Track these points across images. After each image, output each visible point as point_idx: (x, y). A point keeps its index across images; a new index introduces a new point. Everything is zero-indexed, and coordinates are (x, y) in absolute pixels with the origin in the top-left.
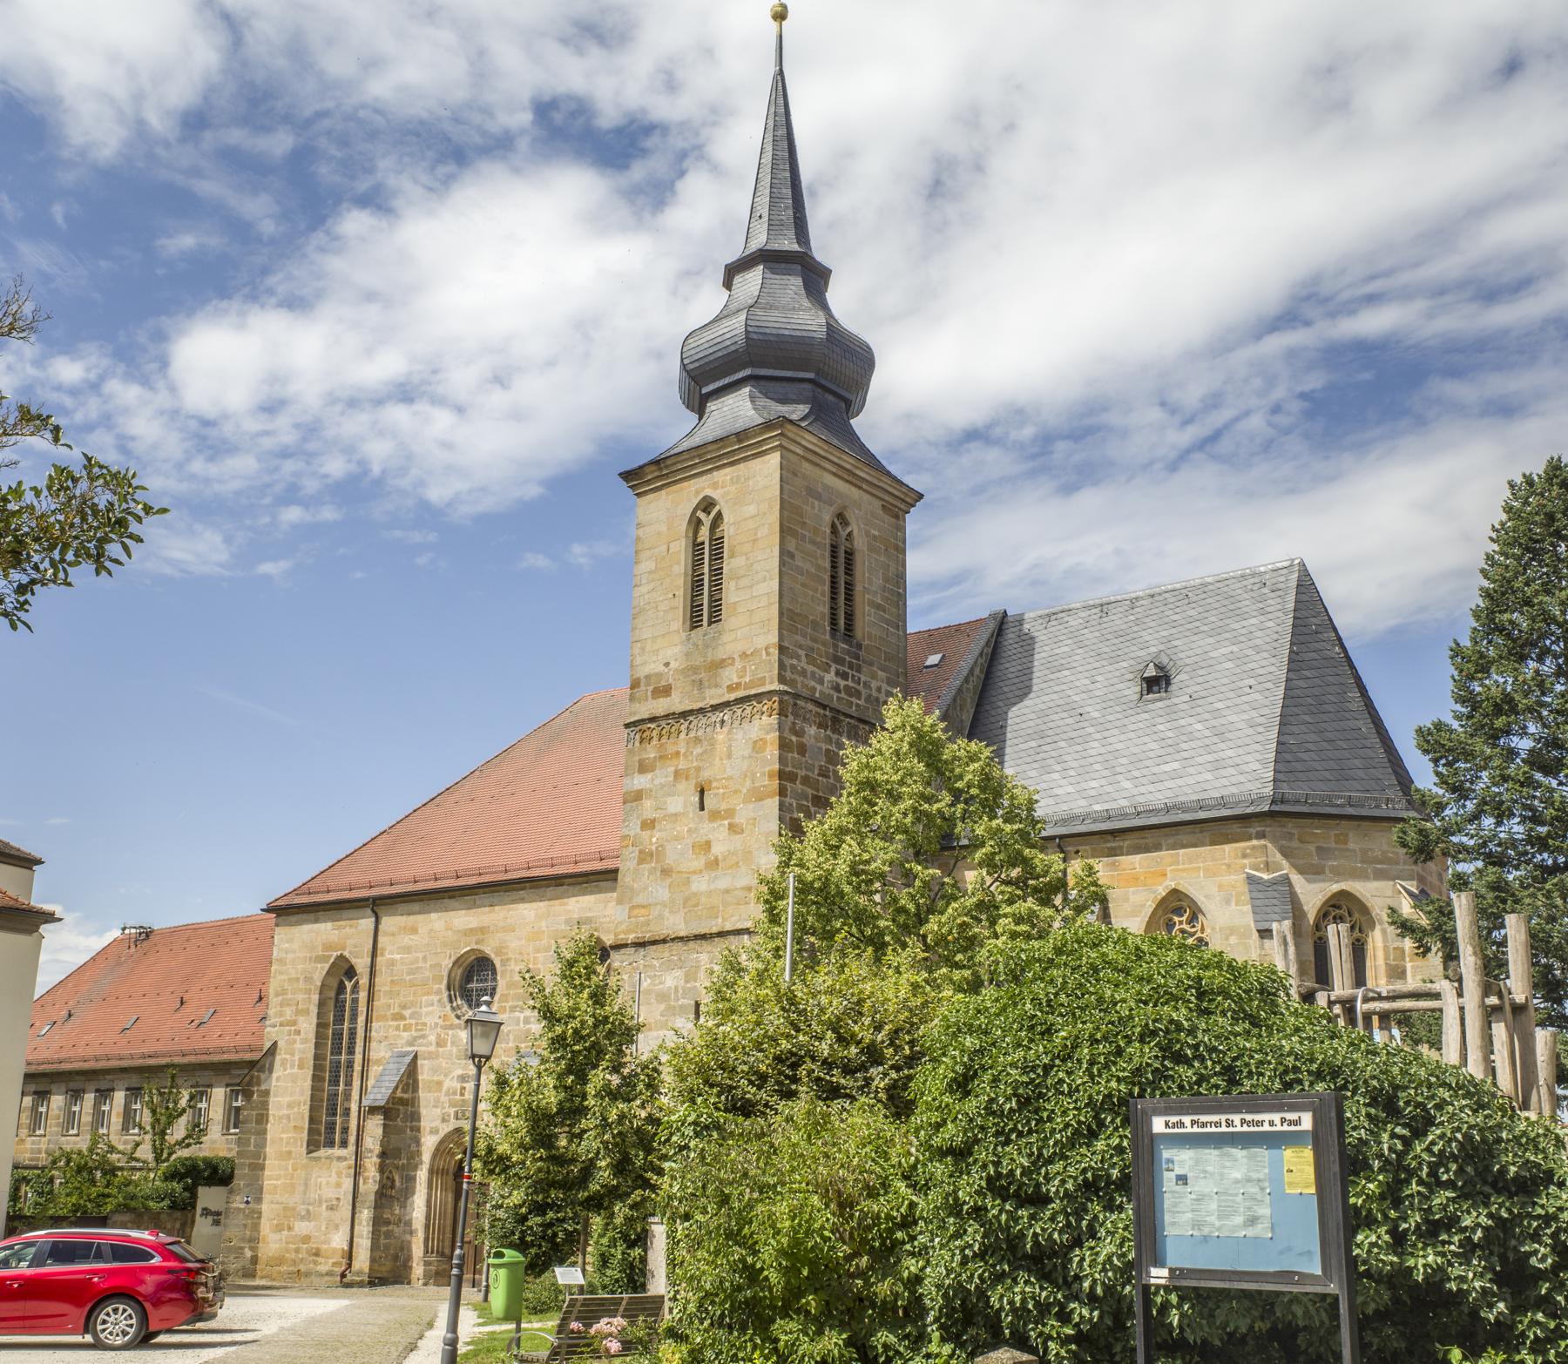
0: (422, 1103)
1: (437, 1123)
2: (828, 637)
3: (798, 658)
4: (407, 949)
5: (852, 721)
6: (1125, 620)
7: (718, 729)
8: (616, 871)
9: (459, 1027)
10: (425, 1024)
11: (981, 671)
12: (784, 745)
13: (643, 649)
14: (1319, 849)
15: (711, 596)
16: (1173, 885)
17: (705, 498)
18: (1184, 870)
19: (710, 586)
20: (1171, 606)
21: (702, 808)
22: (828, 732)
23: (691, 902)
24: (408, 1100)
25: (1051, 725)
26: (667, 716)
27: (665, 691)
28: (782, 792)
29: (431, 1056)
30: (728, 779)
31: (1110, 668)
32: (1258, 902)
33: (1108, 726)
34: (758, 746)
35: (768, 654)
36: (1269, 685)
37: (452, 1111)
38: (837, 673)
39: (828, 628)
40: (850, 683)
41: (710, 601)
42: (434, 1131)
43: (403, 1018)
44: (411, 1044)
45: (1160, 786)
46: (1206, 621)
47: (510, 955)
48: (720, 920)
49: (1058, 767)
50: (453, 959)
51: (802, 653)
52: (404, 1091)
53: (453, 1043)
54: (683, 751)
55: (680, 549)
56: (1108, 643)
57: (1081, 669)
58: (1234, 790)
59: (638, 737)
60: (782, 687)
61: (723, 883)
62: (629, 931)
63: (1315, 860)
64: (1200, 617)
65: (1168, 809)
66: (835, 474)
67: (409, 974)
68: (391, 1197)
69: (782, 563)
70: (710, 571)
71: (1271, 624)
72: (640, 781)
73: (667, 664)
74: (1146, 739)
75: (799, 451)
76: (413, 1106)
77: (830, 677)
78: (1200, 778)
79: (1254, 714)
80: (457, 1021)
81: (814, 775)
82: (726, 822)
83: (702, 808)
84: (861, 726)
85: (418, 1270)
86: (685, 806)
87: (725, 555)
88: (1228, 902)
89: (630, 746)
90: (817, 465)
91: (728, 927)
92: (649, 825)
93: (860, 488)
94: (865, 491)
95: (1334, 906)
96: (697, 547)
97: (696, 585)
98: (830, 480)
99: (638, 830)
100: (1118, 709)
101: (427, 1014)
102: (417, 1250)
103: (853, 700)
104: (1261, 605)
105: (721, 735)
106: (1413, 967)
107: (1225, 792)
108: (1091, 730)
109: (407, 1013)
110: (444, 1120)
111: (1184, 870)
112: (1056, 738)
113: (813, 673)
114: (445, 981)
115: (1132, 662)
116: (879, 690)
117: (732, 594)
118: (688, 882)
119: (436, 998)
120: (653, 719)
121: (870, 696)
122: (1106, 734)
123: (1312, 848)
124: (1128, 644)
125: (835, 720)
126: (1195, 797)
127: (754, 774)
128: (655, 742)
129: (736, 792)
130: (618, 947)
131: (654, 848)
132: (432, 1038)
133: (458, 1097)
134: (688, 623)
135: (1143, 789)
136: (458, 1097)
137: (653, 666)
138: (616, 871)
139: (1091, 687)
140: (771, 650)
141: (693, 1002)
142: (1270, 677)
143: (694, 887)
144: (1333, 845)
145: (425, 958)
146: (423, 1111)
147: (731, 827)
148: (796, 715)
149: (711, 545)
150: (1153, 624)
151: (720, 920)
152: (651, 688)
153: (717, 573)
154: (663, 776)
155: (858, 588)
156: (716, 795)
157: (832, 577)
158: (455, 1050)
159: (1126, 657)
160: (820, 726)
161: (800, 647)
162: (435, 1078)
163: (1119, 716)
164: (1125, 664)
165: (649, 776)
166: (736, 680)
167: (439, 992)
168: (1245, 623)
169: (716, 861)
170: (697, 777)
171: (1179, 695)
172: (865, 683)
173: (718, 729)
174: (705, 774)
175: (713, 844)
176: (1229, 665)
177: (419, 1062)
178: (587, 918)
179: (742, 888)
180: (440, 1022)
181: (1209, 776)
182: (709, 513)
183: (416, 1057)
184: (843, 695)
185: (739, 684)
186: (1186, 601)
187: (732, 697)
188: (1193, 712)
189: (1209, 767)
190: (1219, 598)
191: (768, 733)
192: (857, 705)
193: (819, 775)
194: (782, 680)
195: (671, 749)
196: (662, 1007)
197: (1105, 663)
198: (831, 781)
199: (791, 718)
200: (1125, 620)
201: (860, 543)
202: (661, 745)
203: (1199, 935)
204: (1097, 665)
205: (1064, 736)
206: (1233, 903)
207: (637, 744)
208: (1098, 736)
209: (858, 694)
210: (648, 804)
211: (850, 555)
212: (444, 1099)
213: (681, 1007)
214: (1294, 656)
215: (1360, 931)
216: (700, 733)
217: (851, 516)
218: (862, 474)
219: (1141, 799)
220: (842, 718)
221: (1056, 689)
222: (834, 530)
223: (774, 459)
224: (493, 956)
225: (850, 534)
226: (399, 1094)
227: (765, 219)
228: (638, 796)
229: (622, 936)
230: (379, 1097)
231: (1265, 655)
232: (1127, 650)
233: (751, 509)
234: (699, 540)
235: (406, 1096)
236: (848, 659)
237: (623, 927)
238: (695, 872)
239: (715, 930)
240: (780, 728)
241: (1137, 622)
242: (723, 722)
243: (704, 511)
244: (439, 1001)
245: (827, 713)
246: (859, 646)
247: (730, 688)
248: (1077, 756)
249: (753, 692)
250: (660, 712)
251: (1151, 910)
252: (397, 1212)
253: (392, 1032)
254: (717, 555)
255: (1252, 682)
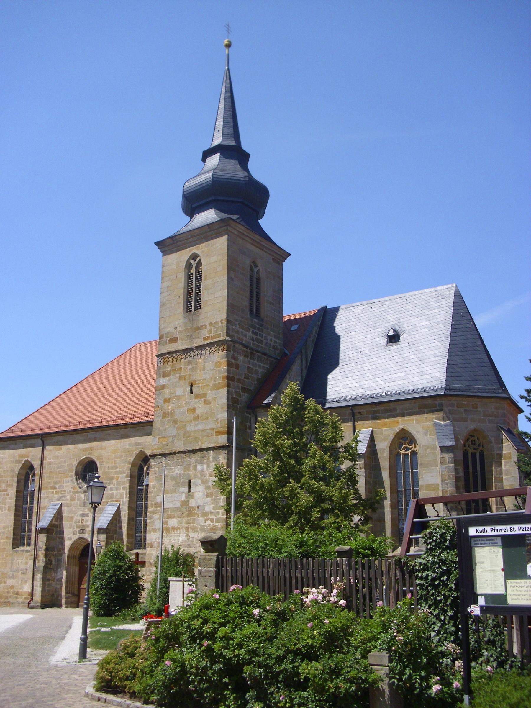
0: (64, 527)
1: (71, 535)
2: (249, 316)
3: (235, 325)
4: (57, 457)
5: (259, 354)
6: (380, 310)
7: (199, 357)
8: (152, 422)
9: (80, 492)
10: (65, 491)
11: (316, 333)
12: (229, 364)
13: (165, 321)
14: (465, 410)
15: (196, 298)
16: (402, 427)
17: (194, 253)
18: (407, 420)
19: (196, 293)
20: (400, 304)
21: (192, 393)
22: (249, 359)
23: (186, 435)
24: (57, 525)
25: (347, 356)
26: (175, 352)
27: (175, 340)
28: (228, 386)
29: (68, 505)
30: (204, 380)
31: (373, 331)
32: (439, 434)
33: (373, 357)
34: (217, 365)
35: (222, 323)
36: (443, 339)
37: (78, 530)
38: (253, 332)
39: (249, 312)
40: (258, 337)
41: (196, 300)
42: (70, 539)
43: (55, 488)
44: (59, 500)
45: (395, 383)
46: (415, 311)
47: (104, 460)
48: (200, 443)
49: (351, 375)
50: (78, 461)
51: (237, 323)
52: (56, 521)
53: (78, 499)
54: (183, 367)
55: (182, 275)
56: (372, 320)
57: (360, 332)
58: (429, 385)
59: (162, 361)
60: (228, 338)
61: (200, 427)
62: (157, 449)
63: (464, 415)
64: (412, 309)
65: (400, 394)
66: (252, 244)
67: (58, 468)
68: (51, 568)
69: (228, 283)
70: (196, 286)
71: (443, 312)
72: (163, 381)
73: (176, 328)
74: (390, 362)
75: (236, 232)
76: (60, 527)
77: (250, 334)
78: (413, 380)
79: (436, 351)
80: (80, 490)
81: (242, 378)
82: (202, 399)
83: (192, 393)
84: (263, 356)
85: (64, 601)
86: (184, 392)
87: (202, 279)
88: (426, 434)
89: (159, 365)
90: (243, 239)
91: (204, 446)
92: (167, 401)
93: (263, 250)
94: (265, 252)
95: (471, 436)
96: (189, 275)
97: (188, 293)
98: (249, 246)
99: (163, 404)
100: (377, 349)
101: (66, 486)
102: (63, 592)
103: (260, 344)
104: (438, 304)
105: (200, 360)
106: (505, 462)
107: (424, 386)
108: (365, 358)
109: (57, 486)
110: (74, 534)
111: (407, 420)
112: (349, 362)
113: (242, 332)
114: (74, 472)
115: (383, 329)
116: (271, 340)
117: (205, 296)
118: (185, 426)
119: (70, 479)
120: (169, 353)
121: (267, 343)
122: (372, 360)
123: (462, 410)
124: (381, 321)
125: (252, 354)
126: (412, 388)
127: (215, 378)
128: (170, 363)
129: (207, 385)
130: (153, 456)
131: (170, 411)
132: (68, 497)
133: (80, 524)
134: (185, 309)
135: (388, 385)
136: (80, 524)
137: (169, 329)
138: (152, 422)
139: (365, 340)
140: (223, 322)
141: (187, 481)
142: (443, 335)
143: (188, 428)
144: (471, 409)
145: (65, 462)
146: (65, 530)
147: (205, 401)
148: (234, 351)
149: (196, 275)
150: (392, 312)
151: (200, 443)
152: (168, 339)
153: (199, 287)
154: (174, 378)
155: (262, 294)
156: (198, 387)
157: (250, 289)
158: (79, 502)
159: (380, 327)
160: (245, 356)
161: (236, 320)
162: (70, 515)
163: (377, 352)
164: (379, 330)
165: (168, 378)
166: (207, 335)
167: (71, 476)
168: (432, 312)
169: (198, 417)
170: (189, 379)
171: (394, 347)
172: (265, 337)
173: (199, 357)
174: (193, 378)
175: (197, 409)
176: (425, 330)
177: (63, 508)
178: (139, 443)
179: (210, 429)
180: (72, 490)
181: (417, 379)
182: (195, 261)
183: (61, 506)
184: (255, 342)
185: (208, 337)
186: (406, 302)
187: (206, 342)
188: (410, 351)
189: (417, 375)
190: (420, 301)
191: (222, 359)
192: (262, 347)
193: (245, 378)
194: (228, 335)
195: (177, 366)
196: (173, 483)
197: (371, 329)
198: (250, 381)
199: (232, 352)
200: (380, 310)
201: (263, 275)
202: (173, 365)
203: (413, 449)
204: (367, 330)
205: (353, 361)
206: (428, 435)
207: (162, 364)
208: (368, 361)
209: (261, 342)
210: (166, 391)
211: (258, 280)
212: (74, 524)
213: (182, 482)
214: (453, 326)
215: (483, 446)
216: (191, 359)
217: (259, 262)
218: (264, 244)
219: (388, 389)
220: (254, 352)
221: (349, 340)
222: (251, 269)
223: (225, 237)
224: (96, 460)
225: (258, 271)
226: (54, 522)
227: (221, 131)
228: (163, 387)
229: (155, 451)
230: (103, 524)
231: (441, 326)
232: (380, 324)
233: (214, 259)
234: (192, 272)
235: (56, 523)
236: (257, 326)
237: (156, 447)
238: (188, 422)
239: (197, 448)
240: (227, 357)
241: (385, 311)
242: (201, 354)
243: (193, 259)
244: (72, 480)
245: (248, 350)
246: (262, 320)
247: (205, 339)
248: (359, 370)
249: (215, 340)
250: (173, 350)
251: (392, 438)
252: (53, 575)
253: (50, 495)
254: (199, 279)
255: (436, 337)
